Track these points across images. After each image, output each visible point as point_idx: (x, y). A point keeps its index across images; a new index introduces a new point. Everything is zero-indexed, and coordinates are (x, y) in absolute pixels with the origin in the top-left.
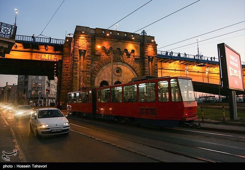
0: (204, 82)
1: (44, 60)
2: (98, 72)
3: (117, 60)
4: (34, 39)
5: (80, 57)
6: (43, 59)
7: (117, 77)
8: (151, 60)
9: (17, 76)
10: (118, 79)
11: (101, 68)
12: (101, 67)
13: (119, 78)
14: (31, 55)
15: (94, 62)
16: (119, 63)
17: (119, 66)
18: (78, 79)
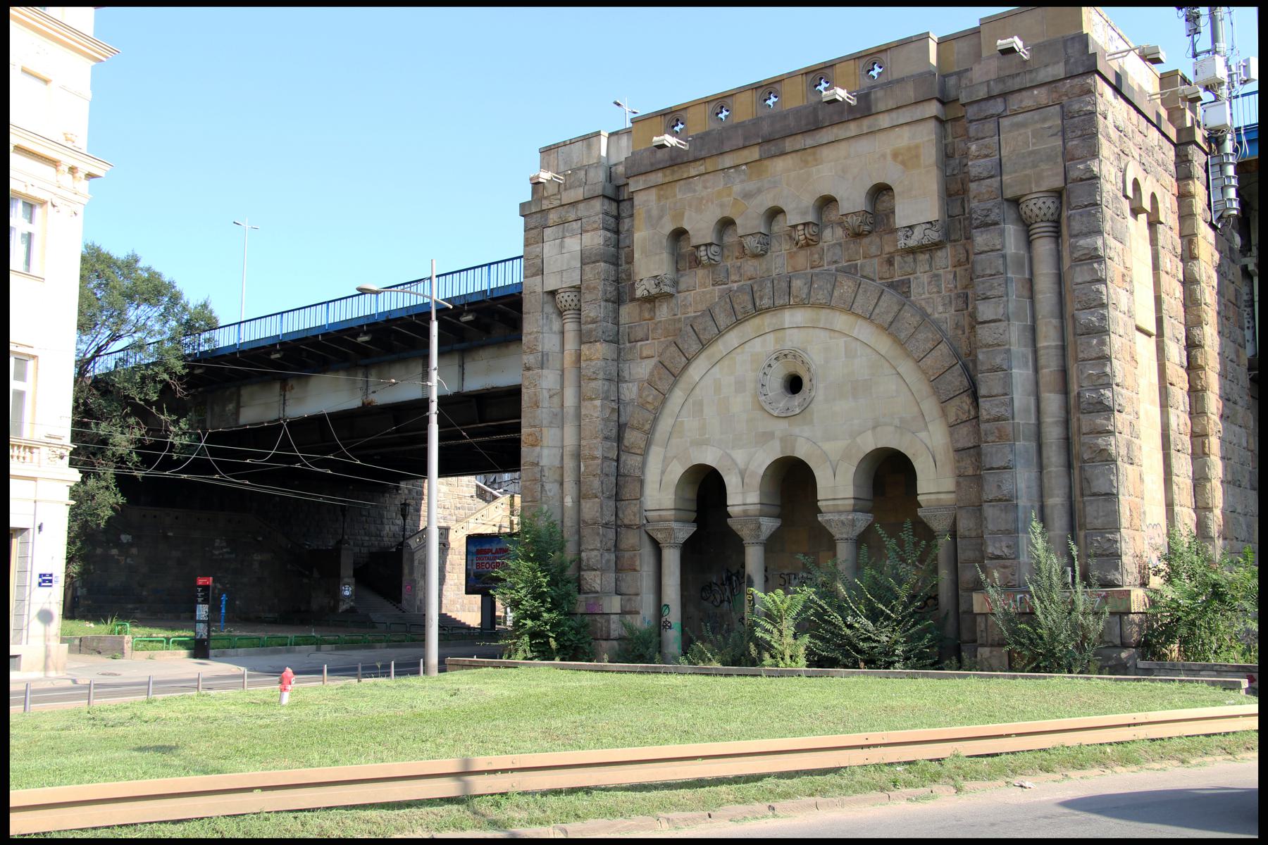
7: (780, 427)
17: (793, 339)
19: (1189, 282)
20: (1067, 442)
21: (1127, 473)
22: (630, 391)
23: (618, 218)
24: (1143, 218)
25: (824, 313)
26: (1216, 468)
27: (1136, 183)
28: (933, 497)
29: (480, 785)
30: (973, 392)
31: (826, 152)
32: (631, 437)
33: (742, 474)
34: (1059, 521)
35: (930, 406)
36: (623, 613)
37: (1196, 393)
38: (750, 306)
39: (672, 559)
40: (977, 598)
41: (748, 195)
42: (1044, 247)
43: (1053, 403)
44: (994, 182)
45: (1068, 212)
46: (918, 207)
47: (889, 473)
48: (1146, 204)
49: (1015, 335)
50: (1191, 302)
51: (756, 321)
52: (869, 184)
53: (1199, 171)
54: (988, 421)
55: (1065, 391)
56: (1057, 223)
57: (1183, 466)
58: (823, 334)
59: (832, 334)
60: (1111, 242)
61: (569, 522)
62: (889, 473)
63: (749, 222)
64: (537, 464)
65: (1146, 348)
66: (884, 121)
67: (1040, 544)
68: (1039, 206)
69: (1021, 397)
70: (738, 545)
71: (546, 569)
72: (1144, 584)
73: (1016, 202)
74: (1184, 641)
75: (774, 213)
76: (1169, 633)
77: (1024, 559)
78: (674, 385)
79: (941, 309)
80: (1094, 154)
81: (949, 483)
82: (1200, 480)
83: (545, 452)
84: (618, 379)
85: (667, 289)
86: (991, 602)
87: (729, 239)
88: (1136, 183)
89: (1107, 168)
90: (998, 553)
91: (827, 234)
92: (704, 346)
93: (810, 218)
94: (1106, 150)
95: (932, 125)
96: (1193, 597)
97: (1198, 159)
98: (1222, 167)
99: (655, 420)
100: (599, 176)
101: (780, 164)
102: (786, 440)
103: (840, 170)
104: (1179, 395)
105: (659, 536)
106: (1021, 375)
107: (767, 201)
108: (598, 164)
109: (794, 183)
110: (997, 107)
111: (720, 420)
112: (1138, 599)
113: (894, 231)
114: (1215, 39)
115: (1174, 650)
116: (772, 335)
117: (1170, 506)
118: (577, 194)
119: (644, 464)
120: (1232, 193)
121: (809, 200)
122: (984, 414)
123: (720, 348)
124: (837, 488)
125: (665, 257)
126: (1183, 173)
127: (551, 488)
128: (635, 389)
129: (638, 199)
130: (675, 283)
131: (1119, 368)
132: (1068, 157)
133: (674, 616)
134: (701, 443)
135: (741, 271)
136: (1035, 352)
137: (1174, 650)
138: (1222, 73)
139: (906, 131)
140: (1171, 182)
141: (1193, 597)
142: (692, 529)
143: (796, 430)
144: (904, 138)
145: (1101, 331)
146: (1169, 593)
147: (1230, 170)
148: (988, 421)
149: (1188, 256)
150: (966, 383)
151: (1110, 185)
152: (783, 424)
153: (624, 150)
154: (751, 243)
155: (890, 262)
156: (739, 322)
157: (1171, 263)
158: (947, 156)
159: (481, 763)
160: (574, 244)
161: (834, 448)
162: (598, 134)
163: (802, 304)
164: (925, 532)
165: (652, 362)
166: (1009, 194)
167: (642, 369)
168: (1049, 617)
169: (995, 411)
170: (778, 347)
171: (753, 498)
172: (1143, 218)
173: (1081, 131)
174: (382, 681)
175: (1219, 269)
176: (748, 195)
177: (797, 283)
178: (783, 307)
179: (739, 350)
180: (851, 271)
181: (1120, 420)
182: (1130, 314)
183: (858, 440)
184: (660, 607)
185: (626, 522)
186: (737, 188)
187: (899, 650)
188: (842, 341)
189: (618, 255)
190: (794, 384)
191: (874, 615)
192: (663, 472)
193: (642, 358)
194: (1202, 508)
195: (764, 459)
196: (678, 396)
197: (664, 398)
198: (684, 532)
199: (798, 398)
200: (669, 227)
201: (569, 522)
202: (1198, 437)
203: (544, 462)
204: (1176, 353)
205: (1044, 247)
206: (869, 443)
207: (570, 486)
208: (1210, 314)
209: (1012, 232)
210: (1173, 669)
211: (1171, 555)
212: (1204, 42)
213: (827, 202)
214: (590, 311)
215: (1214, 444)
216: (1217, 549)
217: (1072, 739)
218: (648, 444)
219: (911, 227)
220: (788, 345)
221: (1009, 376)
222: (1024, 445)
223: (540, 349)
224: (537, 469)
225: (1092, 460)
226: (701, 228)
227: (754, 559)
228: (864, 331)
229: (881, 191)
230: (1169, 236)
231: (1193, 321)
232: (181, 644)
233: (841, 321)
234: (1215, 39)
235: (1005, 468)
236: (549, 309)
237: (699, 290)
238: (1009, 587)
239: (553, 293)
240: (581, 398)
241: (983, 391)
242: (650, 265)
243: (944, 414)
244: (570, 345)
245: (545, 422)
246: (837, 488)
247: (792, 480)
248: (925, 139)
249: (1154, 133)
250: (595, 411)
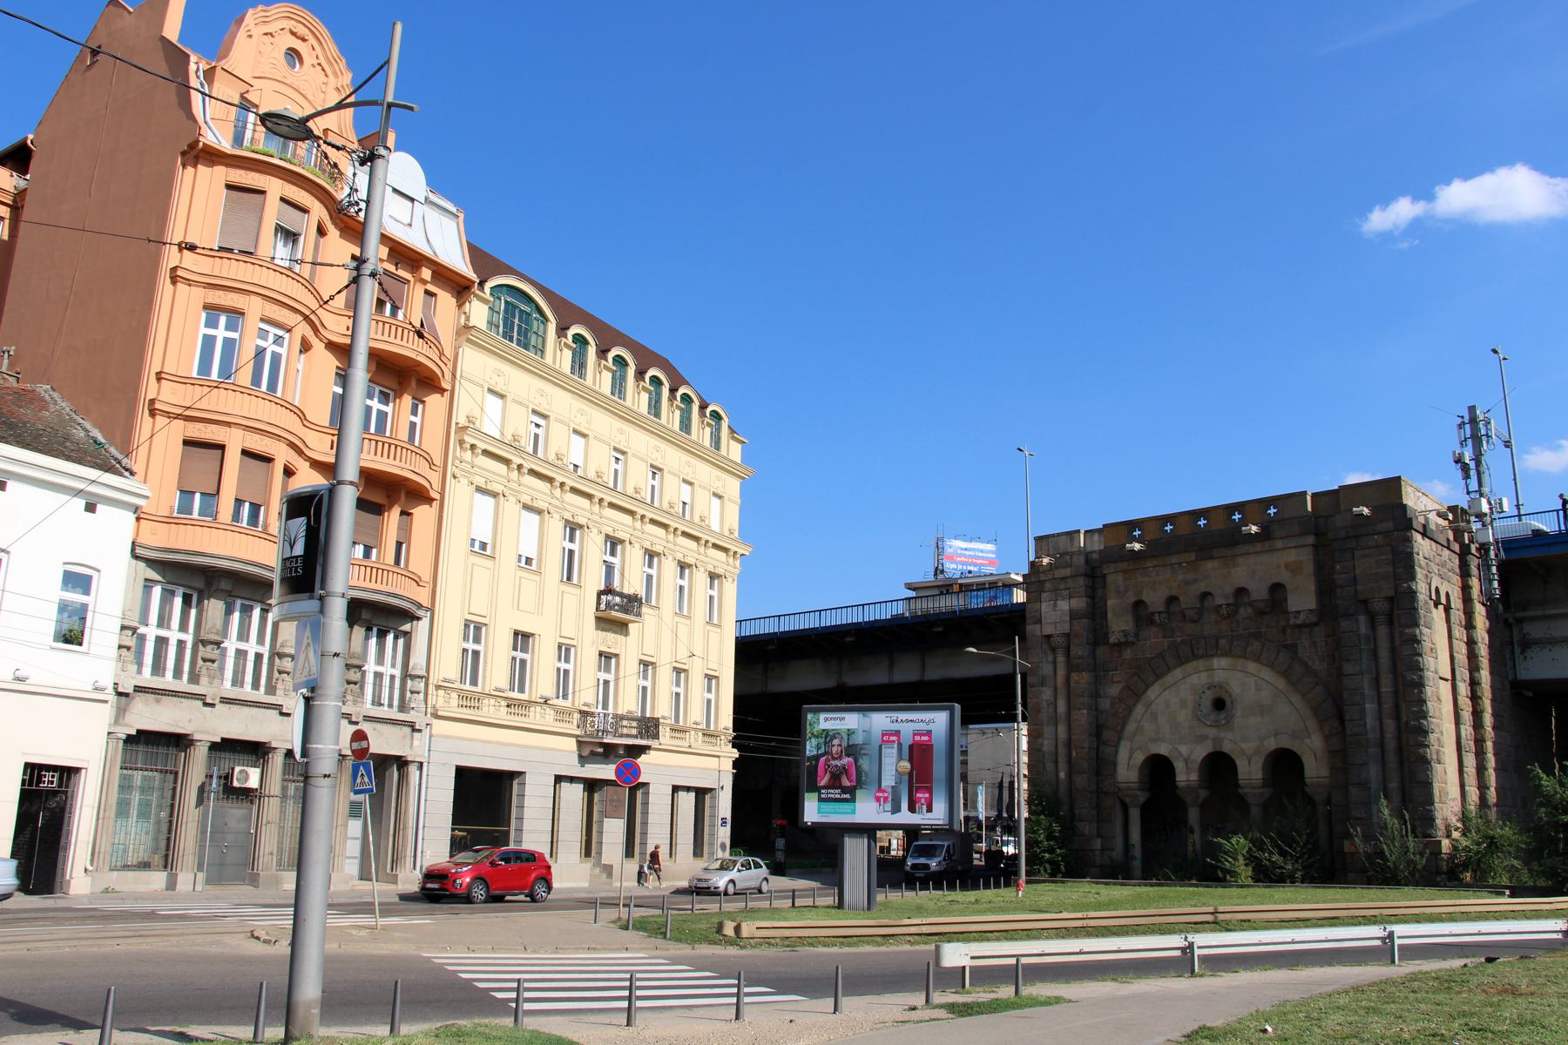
7: (1212, 732)
10: (1215, 740)
13: (1223, 735)
17: (1220, 676)
19: (1471, 643)
20: (1400, 750)
21: (1437, 767)
22: (1105, 704)
23: (1093, 588)
24: (1441, 607)
25: (1241, 661)
26: (1491, 761)
27: (1437, 590)
29: (1221, 917)
30: (1341, 718)
31: (1240, 560)
32: (1107, 734)
33: (1186, 761)
34: (1396, 798)
35: (1312, 724)
36: (1103, 849)
37: (1477, 714)
38: (1191, 651)
39: (1135, 814)
40: (1346, 844)
41: (1187, 583)
43: (1390, 725)
45: (1400, 612)
46: (1302, 600)
48: (1443, 600)
49: (1368, 690)
50: (1472, 656)
51: (1194, 663)
52: (1269, 583)
53: (1474, 571)
55: (1398, 718)
57: (1470, 761)
58: (1240, 675)
60: (1425, 630)
61: (1063, 789)
62: (1284, 764)
63: (1188, 600)
65: (1445, 689)
66: (1279, 544)
67: (1386, 812)
68: (1379, 606)
69: (1370, 721)
70: (1182, 806)
71: (1058, 819)
72: (1448, 836)
73: (1365, 602)
74: (1474, 871)
75: (1205, 595)
76: (1465, 866)
77: (1375, 820)
78: (1137, 701)
80: (1413, 578)
81: (1325, 772)
82: (1481, 769)
84: (1096, 695)
85: (1132, 639)
86: (1357, 844)
87: (1175, 608)
88: (1437, 590)
89: (1421, 586)
91: (1242, 610)
93: (1231, 601)
94: (1420, 574)
95: (1310, 549)
96: (1479, 844)
97: (1474, 563)
98: (1489, 568)
99: (1124, 724)
100: (1079, 561)
101: (1210, 565)
102: (1215, 740)
103: (1252, 573)
104: (1466, 715)
105: (1127, 800)
106: (1370, 707)
107: (1202, 587)
108: (1080, 552)
109: (1222, 578)
111: (1168, 723)
112: (1445, 843)
113: (1286, 612)
114: (1480, 484)
115: (1468, 876)
117: (1462, 786)
118: (1067, 572)
119: (1116, 752)
120: (1496, 584)
121: (1229, 590)
122: (1348, 731)
123: (1169, 679)
124: (1250, 771)
125: (1130, 617)
126: (1465, 573)
127: (1050, 766)
129: (1110, 578)
130: (1137, 635)
131: (1431, 706)
132: (1396, 577)
133: (1137, 852)
134: (1156, 740)
135: (1185, 633)
136: (1379, 694)
137: (1468, 876)
138: (1485, 508)
139: (1293, 552)
140: (1456, 579)
141: (1479, 844)
142: (1147, 795)
143: (1223, 735)
144: (1292, 556)
145: (1420, 685)
146: (1465, 842)
147: (1494, 569)
149: (1469, 626)
150: (1334, 710)
151: (1422, 596)
153: (1097, 544)
154: (1190, 613)
155: (1284, 631)
156: (1182, 664)
157: (1460, 633)
158: (1319, 568)
159: (1221, 909)
160: (1064, 605)
162: (1078, 531)
163: (1225, 654)
164: (1309, 800)
165: (1120, 686)
166: (1361, 597)
167: (1114, 690)
168: (1392, 853)
171: (1194, 777)
172: (1441, 607)
173: (1404, 565)
174: (1006, 893)
175: (1489, 632)
176: (1187, 583)
177: (1223, 642)
180: (1257, 636)
181: (1432, 737)
182: (1436, 672)
184: (1127, 846)
186: (1180, 577)
187: (1298, 875)
188: (1252, 680)
189: (1095, 614)
190: (1219, 704)
191: (1283, 853)
194: (1482, 787)
195: (1201, 752)
196: (1139, 709)
197: (1130, 710)
198: (1143, 797)
199: (1222, 715)
200: (1133, 599)
201: (1063, 789)
202: (1479, 741)
203: (1045, 749)
204: (1463, 689)
205: (1382, 631)
206: (1272, 744)
207: (1062, 765)
208: (1484, 662)
209: (1362, 618)
210: (1468, 886)
211: (1464, 818)
212: (1474, 485)
213: (1241, 591)
214: (1078, 651)
215: (1489, 745)
216: (1493, 814)
217: (1428, 910)
218: (1120, 739)
220: (1216, 680)
221: (1364, 709)
222: (1373, 750)
226: (1155, 599)
227: (1193, 815)
228: (1267, 674)
229: (1277, 588)
230: (1458, 615)
231: (1474, 667)
233: (1252, 667)
234: (1480, 484)
236: (1045, 647)
237: (1153, 641)
238: (1367, 837)
239: (1049, 637)
240: (1069, 708)
241: (1347, 717)
242: (1119, 624)
243: (1321, 729)
244: (1061, 673)
246: (1250, 771)
247: (1219, 766)
248: (1305, 557)
249: (1446, 552)
250: (1082, 717)
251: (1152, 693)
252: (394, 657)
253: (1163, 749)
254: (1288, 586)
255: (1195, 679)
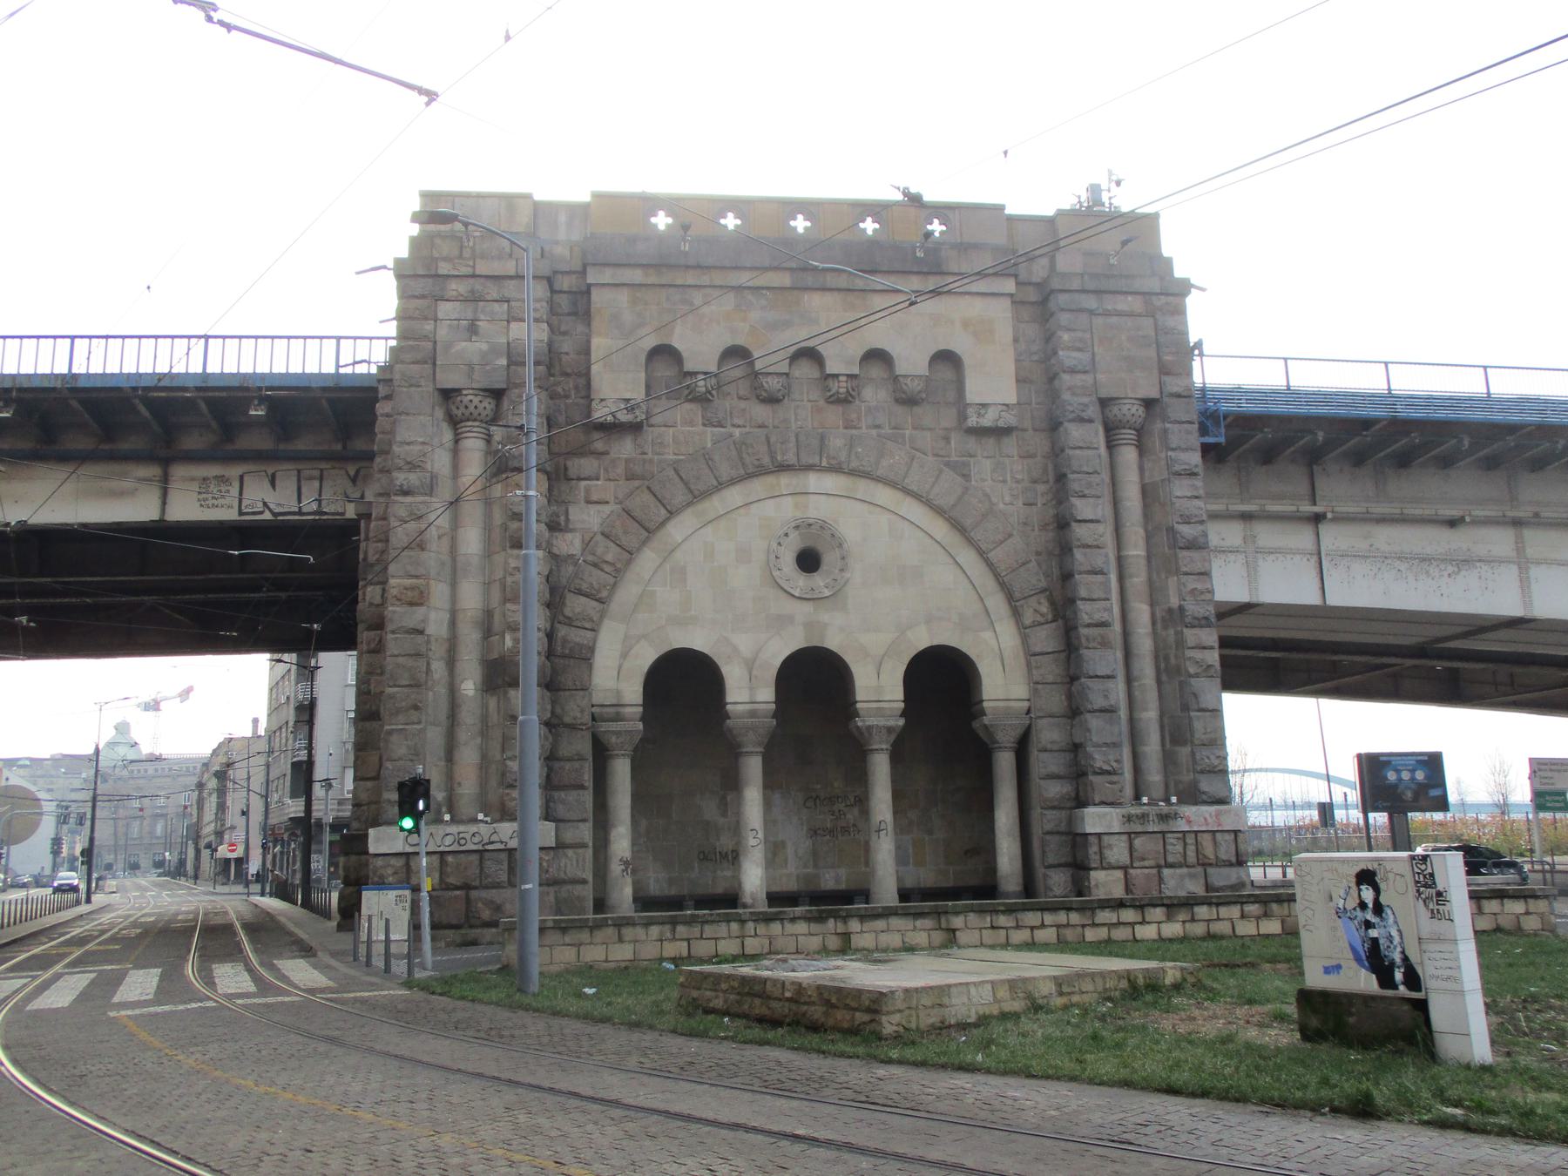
0: (1334, 600)
1: (267, 516)
2: (618, 573)
3: (791, 458)
4: (1520, 549)
5: (455, 452)
6: (260, 507)
7: (803, 610)
8: (1129, 434)
9: (268, 656)
10: (809, 626)
11: (644, 543)
12: (651, 531)
13: (825, 617)
14: (165, 483)
15: (587, 490)
16: (814, 481)
17: (818, 509)
18: (438, 651)
28: (1001, 704)
32: (576, 605)
33: (750, 665)
39: (621, 771)
42: (1128, 455)
44: (1089, 378)
46: (993, 385)
47: (941, 678)
54: (1089, 626)
56: (1140, 432)
59: (872, 508)
62: (941, 678)
64: (421, 632)
79: (1007, 499)
83: (433, 616)
90: (1106, 767)
92: (697, 497)
110: (1090, 302)
116: (789, 498)
123: (715, 504)
124: (879, 689)
128: (577, 543)
148: (1089, 626)
152: (807, 607)
161: (877, 641)
169: (1097, 617)
170: (799, 514)
171: (766, 694)
178: (810, 468)
179: (742, 511)
183: (909, 633)
185: (567, 720)
188: (885, 518)
190: (808, 561)
192: (624, 655)
193: (589, 502)
196: (648, 560)
199: (818, 580)
203: (431, 630)
205: (1128, 455)
213: (877, 356)
219: (984, 405)
223: (429, 467)
224: (420, 639)
225: (1197, 675)
226: (700, 348)
232: (745, 906)
235: (1109, 677)
237: (679, 431)
245: (433, 573)
246: (879, 689)
247: (815, 679)
248: (1000, 314)
251: (677, 530)
252: (837, 968)
253: (698, 641)
254: (967, 361)
255: (769, 508)
